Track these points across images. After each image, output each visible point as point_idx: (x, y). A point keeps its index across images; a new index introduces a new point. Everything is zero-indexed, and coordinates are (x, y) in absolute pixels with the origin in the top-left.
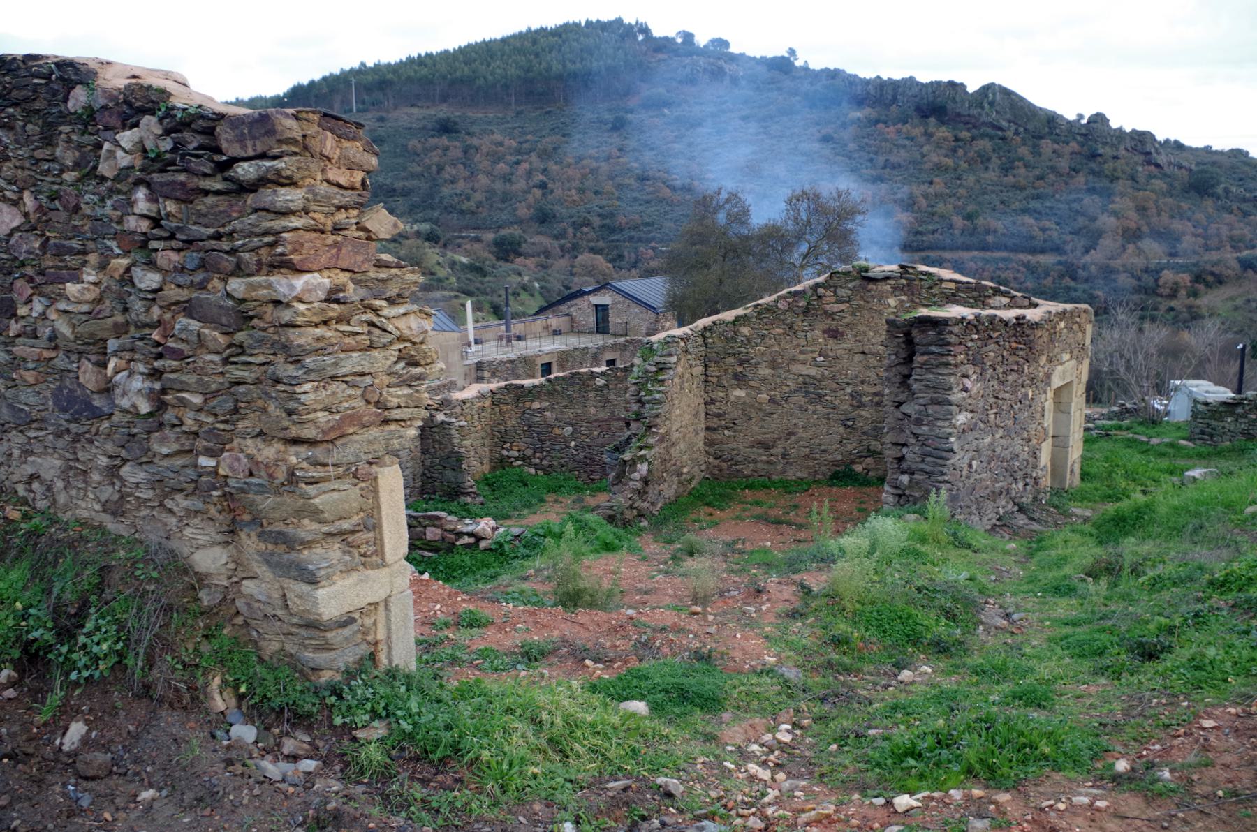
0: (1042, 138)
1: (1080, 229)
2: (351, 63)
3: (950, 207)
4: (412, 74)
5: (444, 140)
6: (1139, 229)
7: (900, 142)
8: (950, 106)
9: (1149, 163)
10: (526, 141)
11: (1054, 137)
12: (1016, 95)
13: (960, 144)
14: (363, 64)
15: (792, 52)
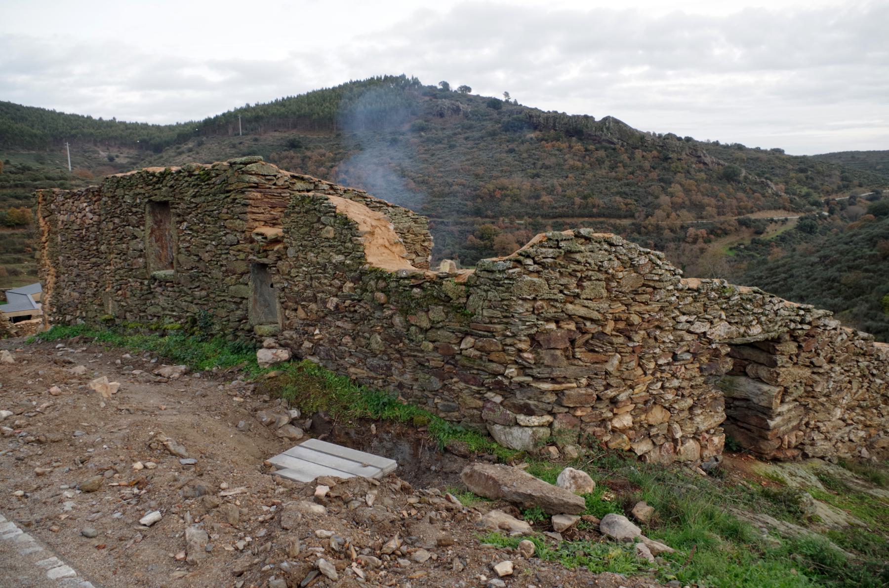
0: (637, 148)
1: (649, 204)
2: (240, 104)
3: (574, 192)
4: (275, 111)
5: (292, 153)
6: (684, 203)
7: (553, 152)
8: (585, 130)
9: (700, 162)
10: (339, 153)
11: (643, 148)
12: (623, 123)
13: (587, 153)
14: (248, 105)
15: (114, 118)
